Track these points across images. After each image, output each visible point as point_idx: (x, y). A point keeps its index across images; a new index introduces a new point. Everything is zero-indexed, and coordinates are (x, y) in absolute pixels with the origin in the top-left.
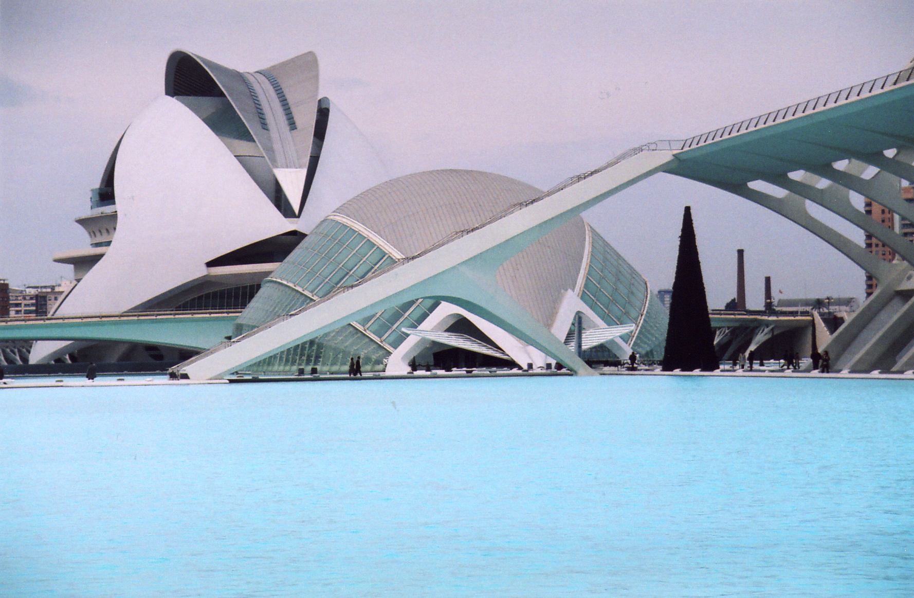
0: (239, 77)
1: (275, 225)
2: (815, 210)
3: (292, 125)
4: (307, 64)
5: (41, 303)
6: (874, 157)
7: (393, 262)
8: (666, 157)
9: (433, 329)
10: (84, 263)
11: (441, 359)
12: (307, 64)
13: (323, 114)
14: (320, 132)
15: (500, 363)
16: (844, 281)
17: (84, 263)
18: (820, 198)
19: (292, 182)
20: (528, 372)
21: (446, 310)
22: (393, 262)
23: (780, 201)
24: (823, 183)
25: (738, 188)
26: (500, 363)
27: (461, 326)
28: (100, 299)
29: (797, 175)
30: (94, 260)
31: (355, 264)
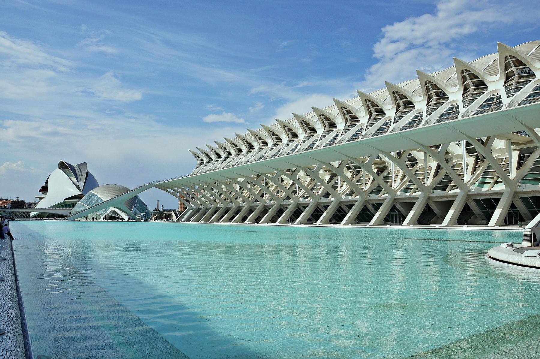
1: (79, 193)
27: (115, 212)
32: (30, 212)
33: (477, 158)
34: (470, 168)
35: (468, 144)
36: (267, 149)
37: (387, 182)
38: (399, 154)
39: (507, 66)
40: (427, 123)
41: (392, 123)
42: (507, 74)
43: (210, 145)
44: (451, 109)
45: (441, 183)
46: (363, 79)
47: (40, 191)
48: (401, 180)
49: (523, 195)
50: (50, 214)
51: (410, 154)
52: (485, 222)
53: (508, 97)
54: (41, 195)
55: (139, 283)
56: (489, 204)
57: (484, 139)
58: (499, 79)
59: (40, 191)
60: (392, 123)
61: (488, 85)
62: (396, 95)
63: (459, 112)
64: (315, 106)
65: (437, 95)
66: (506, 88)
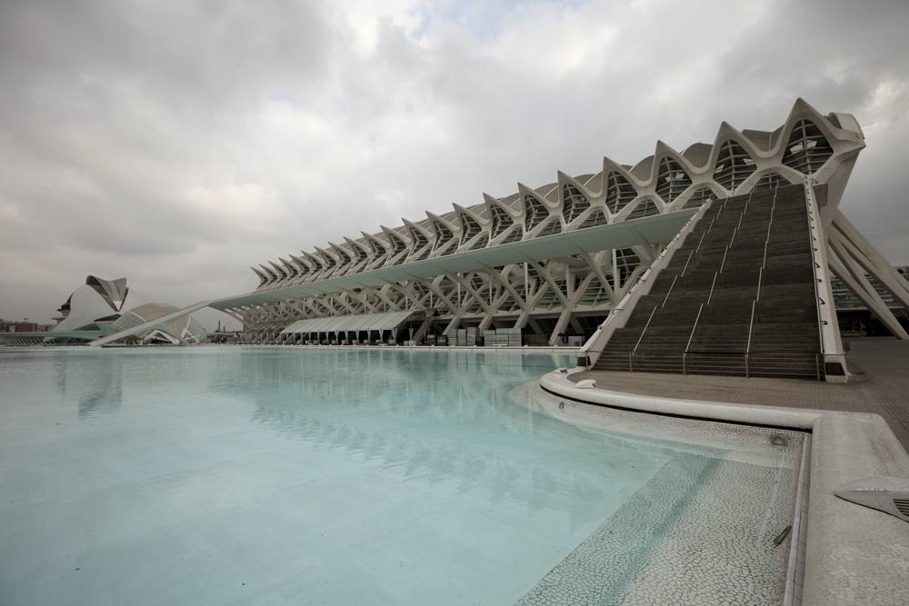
0: (106, 282)
1: (113, 313)
2: (237, 315)
3: (119, 292)
4: (124, 280)
5: (47, 328)
6: (261, 305)
7: (143, 322)
8: (208, 303)
9: (152, 336)
10: (60, 320)
11: (155, 342)
12: (124, 280)
13: (127, 291)
14: (126, 294)
15: (213, 305)
16: (239, 326)
17: (60, 320)
18: (238, 313)
19: (118, 303)
20: (175, 345)
21: (156, 331)
22: (143, 322)
23: (713, 206)
24: (239, 310)
25: (223, 310)
26: (213, 305)
27: (159, 335)
28: (63, 329)
29: (234, 308)
30: (63, 319)
31: (133, 321)
32: (43, 337)
33: (538, 280)
34: (532, 290)
35: (530, 266)
36: (308, 274)
37: (454, 303)
38: (465, 275)
39: (566, 194)
40: (435, 255)
41: (524, 229)
42: (659, 179)
43: (256, 268)
44: (551, 225)
45: (505, 303)
46: (833, 119)
47: (59, 310)
48: (467, 300)
49: (579, 316)
50: (72, 339)
51: (476, 275)
52: (544, 340)
53: (567, 222)
54: (60, 315)
55: (830, 243)
56: (550, 323)
57: (545, 261)
58: (651, 185)
59: (59, 310)
60: (524, 229)
61: (638, 191)
62: (464, 217)
63: (522, 235)
64: (384, 225)
65: (503, 219)
66: (564, 215)
